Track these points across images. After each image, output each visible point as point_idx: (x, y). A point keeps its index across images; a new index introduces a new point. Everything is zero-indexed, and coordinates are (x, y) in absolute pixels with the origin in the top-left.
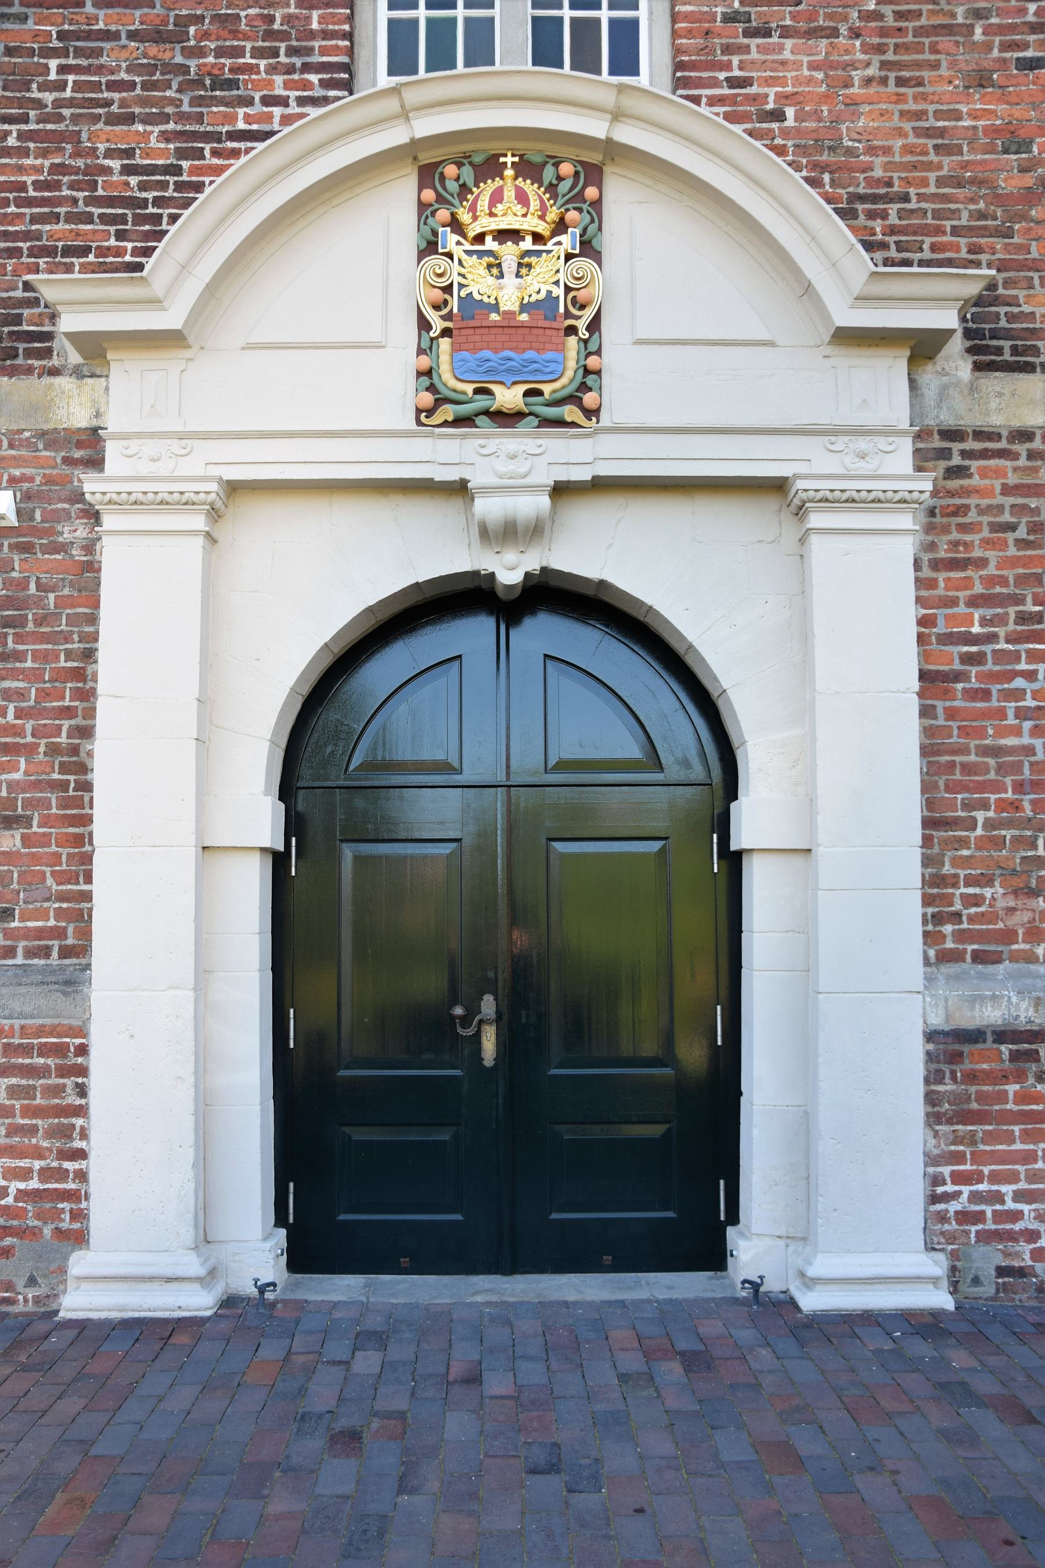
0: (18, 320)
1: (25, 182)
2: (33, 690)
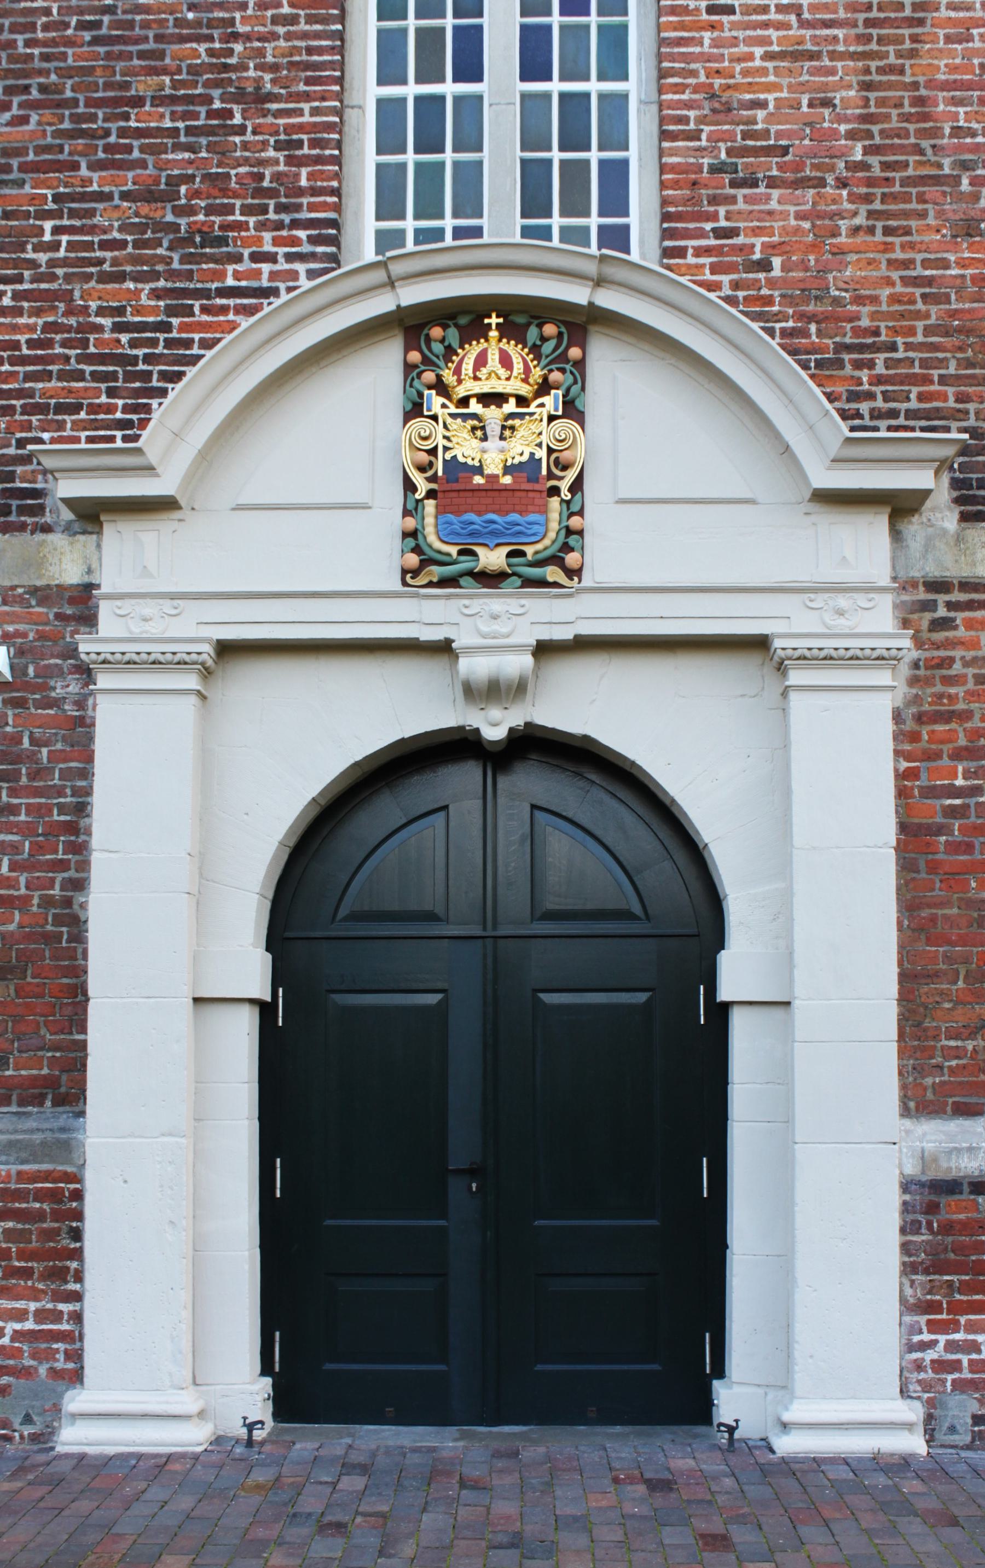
0: (11, 477)
1: (19, 341)
2: (27, 844)
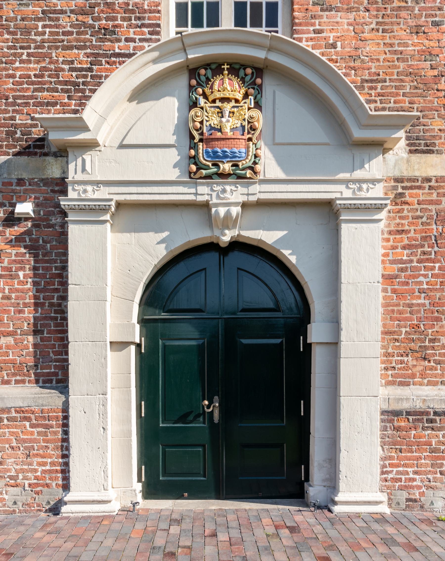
2: (43, 282)
